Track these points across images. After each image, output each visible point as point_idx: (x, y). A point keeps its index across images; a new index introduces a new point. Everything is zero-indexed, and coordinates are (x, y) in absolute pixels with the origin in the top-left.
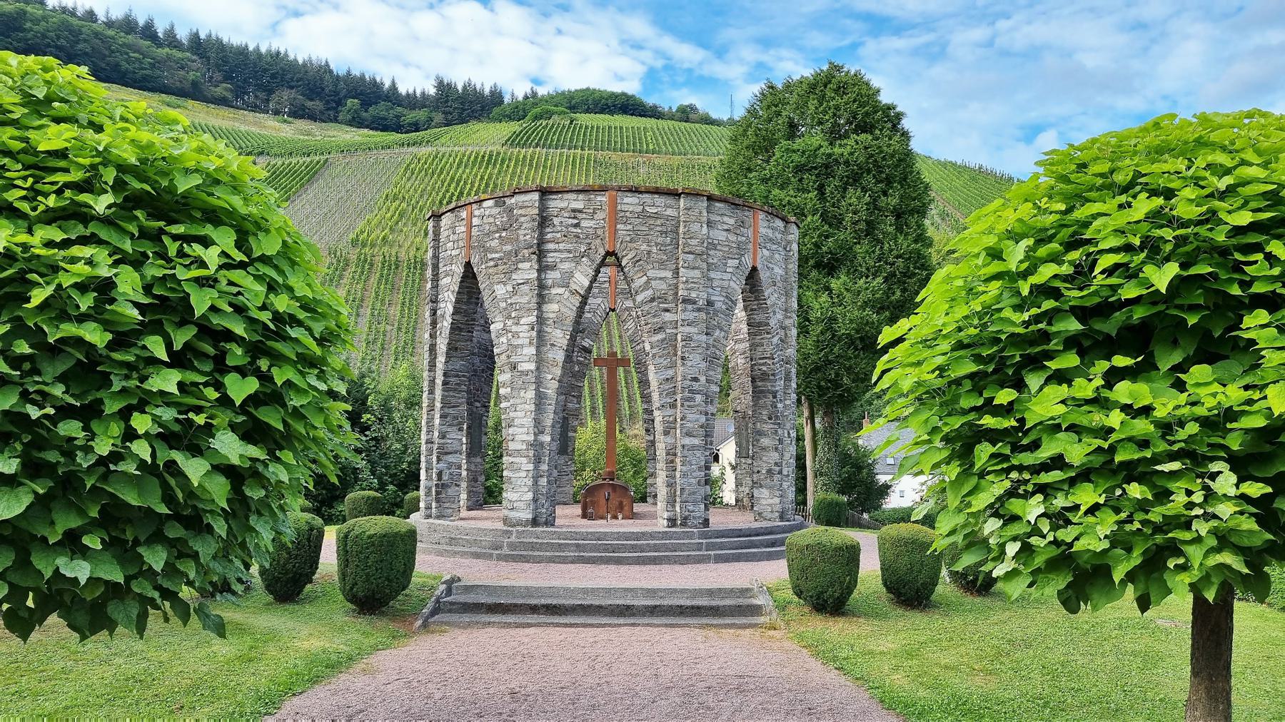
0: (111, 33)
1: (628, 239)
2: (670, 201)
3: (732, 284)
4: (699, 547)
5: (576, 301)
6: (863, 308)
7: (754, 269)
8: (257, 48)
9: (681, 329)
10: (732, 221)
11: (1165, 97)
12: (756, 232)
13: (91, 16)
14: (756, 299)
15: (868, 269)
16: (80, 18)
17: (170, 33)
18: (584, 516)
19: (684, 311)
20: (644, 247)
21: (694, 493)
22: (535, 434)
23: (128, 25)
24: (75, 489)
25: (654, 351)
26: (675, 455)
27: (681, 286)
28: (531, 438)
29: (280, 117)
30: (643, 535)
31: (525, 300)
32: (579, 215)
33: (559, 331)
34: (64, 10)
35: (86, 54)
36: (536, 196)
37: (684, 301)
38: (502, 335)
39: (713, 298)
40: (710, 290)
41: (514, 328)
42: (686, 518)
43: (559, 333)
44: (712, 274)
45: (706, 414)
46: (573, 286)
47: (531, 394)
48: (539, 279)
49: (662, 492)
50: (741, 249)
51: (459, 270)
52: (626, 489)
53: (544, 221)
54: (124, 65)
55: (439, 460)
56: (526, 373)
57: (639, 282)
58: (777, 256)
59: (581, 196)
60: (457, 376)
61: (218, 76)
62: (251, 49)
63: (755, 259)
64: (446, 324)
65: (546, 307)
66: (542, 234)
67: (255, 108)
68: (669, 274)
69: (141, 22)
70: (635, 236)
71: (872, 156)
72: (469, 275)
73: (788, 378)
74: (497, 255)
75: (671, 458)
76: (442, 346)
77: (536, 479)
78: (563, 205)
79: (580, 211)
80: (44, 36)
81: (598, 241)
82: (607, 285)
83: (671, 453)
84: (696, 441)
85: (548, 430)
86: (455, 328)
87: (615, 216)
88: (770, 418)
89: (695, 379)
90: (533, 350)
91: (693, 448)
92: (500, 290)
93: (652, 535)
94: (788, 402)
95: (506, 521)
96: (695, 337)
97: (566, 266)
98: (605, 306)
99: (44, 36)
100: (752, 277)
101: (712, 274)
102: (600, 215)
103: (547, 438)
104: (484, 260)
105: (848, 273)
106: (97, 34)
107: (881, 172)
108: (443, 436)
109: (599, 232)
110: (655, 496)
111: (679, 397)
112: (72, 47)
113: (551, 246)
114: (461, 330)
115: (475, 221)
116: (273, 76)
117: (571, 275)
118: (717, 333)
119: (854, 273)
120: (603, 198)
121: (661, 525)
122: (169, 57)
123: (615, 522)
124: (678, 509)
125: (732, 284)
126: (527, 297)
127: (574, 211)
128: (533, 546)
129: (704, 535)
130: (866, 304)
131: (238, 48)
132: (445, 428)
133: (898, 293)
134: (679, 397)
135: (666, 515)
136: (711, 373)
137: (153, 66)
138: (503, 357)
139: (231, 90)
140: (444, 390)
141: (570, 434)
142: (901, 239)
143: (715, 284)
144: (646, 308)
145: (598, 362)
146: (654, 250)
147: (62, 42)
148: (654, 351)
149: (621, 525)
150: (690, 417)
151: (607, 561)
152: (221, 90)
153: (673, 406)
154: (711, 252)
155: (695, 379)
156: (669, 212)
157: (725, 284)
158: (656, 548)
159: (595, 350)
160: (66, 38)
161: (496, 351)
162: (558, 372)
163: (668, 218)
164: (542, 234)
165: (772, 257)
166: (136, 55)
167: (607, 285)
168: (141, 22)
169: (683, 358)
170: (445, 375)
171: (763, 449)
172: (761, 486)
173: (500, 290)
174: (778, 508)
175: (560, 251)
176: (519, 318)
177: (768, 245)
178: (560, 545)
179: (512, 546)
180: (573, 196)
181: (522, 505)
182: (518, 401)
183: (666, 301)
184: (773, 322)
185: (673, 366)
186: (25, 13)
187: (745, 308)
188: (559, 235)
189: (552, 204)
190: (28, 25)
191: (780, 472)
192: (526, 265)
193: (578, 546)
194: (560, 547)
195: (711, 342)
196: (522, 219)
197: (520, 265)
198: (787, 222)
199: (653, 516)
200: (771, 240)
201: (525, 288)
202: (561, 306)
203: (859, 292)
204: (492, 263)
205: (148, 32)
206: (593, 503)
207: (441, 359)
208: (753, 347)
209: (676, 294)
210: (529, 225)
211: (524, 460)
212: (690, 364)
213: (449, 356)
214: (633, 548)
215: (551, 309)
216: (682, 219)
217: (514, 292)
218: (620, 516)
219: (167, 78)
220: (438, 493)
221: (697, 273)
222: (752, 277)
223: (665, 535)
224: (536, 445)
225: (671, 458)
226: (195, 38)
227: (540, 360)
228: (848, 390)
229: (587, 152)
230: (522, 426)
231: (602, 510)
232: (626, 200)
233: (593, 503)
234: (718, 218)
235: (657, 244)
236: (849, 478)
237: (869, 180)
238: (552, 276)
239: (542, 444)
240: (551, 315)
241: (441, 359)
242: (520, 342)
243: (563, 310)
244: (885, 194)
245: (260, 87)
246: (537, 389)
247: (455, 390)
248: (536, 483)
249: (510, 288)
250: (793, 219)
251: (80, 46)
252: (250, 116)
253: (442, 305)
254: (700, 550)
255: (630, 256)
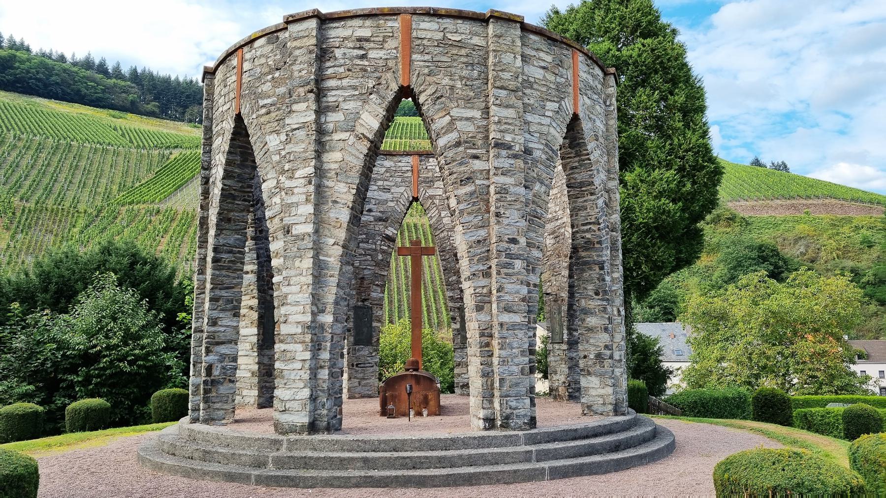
0: (75, 69)
1: (426, 71)
2: (477, 27)
3: (552, 130)
4: (527, 457)
5: (364, 147)
6: (657, 197)
7: (575, 118)
8: (177, 78)
9: (494, 179)
10: (549, 58)
11: (801, 102)
12: (575, 75)
13: (62, 58)
14: (578, 155)
15: (659, 162)
16: (54, 61)
17: (117, 70)
18: (384, 412)
19: (497, 156)
20: (446, 81)
21: (517, 385)
22: (313, 314)
23: (88, 64)
24: (630, 368)
25: (462, 206)
26: (491, 336)
27: (493, 127)
28: (308, 318)
29: (192, 124)
30: (452, 443)
31: (299, 148)
32: (367, 45)
33: (342, 185)
34: (44, 55)
35: (57, 83)
36: (313, 24)
37: (497, 145)
38: (275, 194)
39: (531, 145)
40: (528, 136)
41: (288, 184)
42: (507, 418)
43: (342, 187)
44: (529, 117)
45: (528, 285)
46: (360, 130)
47: (307, 263)
48: (317, 121)
49: (476, 383)
50: (560, 93)
51: (229, 125)
52: (431, 381)
53: (323, 54)
54: (84, 91)
55: (208, 351)
56: (301, 237)
57: (440, 122)
58: (598, 107)
59: (368, 22)
60: (230, 252)
61: (149, 97)
62: (173, 79)
63: (575, 104)
64: (216, 192)
65: (326, 157)
66: (320, 70)
67: (176, 119)
68: (477, 114)
69: (97, 62)
70: (435, 67)
71: (659, 57)
72: (240, 132)
73: (613, 249)
74: (269, 101)
75: (486, 340)
76: (213, 219)
77: (314, 373)
78: (347, 33)
79: (367, 40)
80: (28, 72)
81: (389, 75)
82: (409, 174)
83: (486, 333)
84: (517, 318)
85: (330, 308)
86: (225, 195)
87: (410, 44)
88: (597, 294)
89: (514, 241)
90: (310, 208)
91: (513, 327)
92: (274, 141)
93: (465, 443)
94: (616, 275)
95: (278, 427)
96: (512, 189)
97: (351, 105)
98: (408, 194)
99: (28, 72)
100: (574, 124)
101: (529, 117)
102: (391, 44)
103: (327, 319)
104: (255, 108)
105: (640, 166)
106: (65, 70)
107: (668, 73)
108: (213, 322)
109: (391, 64)
110: (466, 386)
111: (493, 263)
112: (48, 79)
113: (331, 83)
114: (234, 198)
115: (246, 66)
116: (188, 97)
117: (357, 116)
118: (537, 187)
119: (648, 166)
120: (395, 24)
121: (475, 427)
122: (115, 85)
123: (419, 419)
124: (497, 405)
125: (552, 130)
126: (304, 144)
127: (360, 40)
128: (306, 463)
129: (533, 440)
130: (660, 195)
131: (163, 78)
132: (215, 314)
133: (689, 186)
134: (493, 263)
135: (482, 414)
136: (533, 235)
137: (104, 91)
138: (276, 220)
139: (159, 107)
140: (214, 268)
141: (375, 324)
142: (689, 134)
143: (533, 128)
144: (450, 154)
145: (401, 251)
146: (459, 85)
147: (40, 76)
148: (462, 206)
149: (426, 427)
150: (508, 287)
151: (405, 482)
152: (152, 106)
153: (487, 274)
154: (528, 91)
155: (514, 241)
156: (476, 40)
157: (545, 129)
158: (471, 461)
159: (399, 240)
160: (43, 73)
161: (268, 214)
162: (342, 234)
163: (474, 47)
164: (320, 70)
165: (593, 107)
166: (92, 84)
167: (409, 174)
168: (97, 62)
169: (498, 215)
170: (215, 250)
171: (590, 330)
172: (589, 374)
173: (274, 141)
174: (611, 399)
175: (343, 88)
176: (293, 171)
177: (589, 92)
178: (342, 460)
179: (280, 463)
180: (357, 22)
181: (296, 405)
182: (292, 272)
183: (474, 146)
184: (597, 181)
185: (485, 225)
186: (15, 56)
187: (564, 167)
188: (341, 70)
189: (332, 33)
190: (17, 64)
191: (611, 357)
192: (302, 106)
193: (365, 460)
194: (343, 463)
195: (530, 196)
196: (297, 52)
197: (295, 107)
198: (606, 74)
199: (464, 410)
200: (591, 88)
201: (301, 134)
202: (345, 154)
203: (654, 183)
204: (264, 111)
205: (102, 68)
206: (394, 398)
207: (212, 232)
208: (574, 212)
209: (487, 137)
210: (306, 58)
211: (299, 347)
212: (506, 221)
213: (220, 229)
214: (441, 462)
215: (332, 159)
216: (492, 47)
217: (288, 141)
218: (425, 413)
219: (115, 99)
220: (206, 392)
221: (510, 113)
222: (574, 124)
223: (481, 442)
224: (315, 328)
225: (486, 340)
226: (134, 72)
227: (319, 221)
228: (646, 278)
229: (404, 140)
230: (297, 303)
231: (404, 407)
232: (423, 25)
233: (394, 398)
234: (533, 53)
235: (461, 78)
236: (638, 365)
237: (657, 79)
238: (333, 119)
239: (322, 327)
240: (334, 166)
241: (212, 232)
242: (294, 199)
243: (349, 158)
244: (672, 94)
245: (178, 104)
246: (316, 257)
247: (229, 268)
248: (314, 375)
249: (283, 137)
250: (612, 70)
251: (53, 78)
252: (171, 123)
253: (213, 171)
254: (528, 460)
255: (429, 91)
